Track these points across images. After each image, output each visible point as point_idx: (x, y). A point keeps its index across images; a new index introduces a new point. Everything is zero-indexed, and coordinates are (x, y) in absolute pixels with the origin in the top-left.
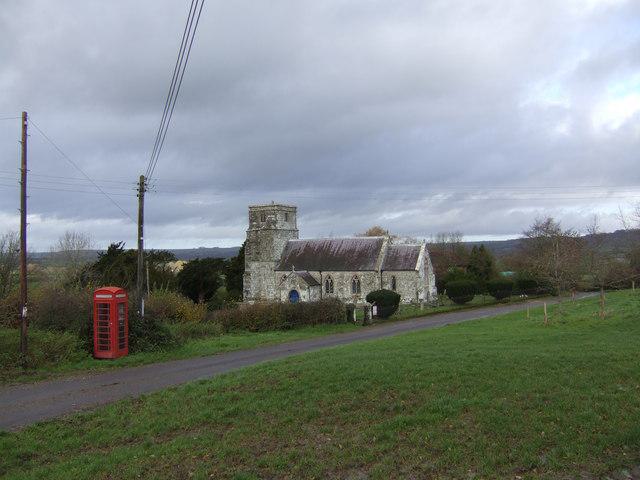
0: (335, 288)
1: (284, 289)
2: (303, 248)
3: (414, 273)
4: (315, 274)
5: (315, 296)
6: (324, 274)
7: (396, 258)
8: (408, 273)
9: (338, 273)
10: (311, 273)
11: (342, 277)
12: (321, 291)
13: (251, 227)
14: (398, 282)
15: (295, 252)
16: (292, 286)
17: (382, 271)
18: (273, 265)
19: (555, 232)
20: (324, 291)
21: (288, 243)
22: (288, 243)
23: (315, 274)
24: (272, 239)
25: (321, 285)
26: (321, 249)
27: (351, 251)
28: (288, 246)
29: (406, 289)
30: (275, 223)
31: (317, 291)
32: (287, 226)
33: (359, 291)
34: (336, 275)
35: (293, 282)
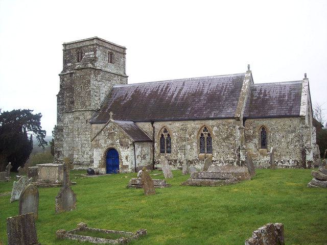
0: (174, 146)
1: (98, 146)
2: (130, 94)
3: (296, 121)
4: (146, 127)
5: (144, 158)
6: (158, 125)
7: (256, 89)
8: (287, 121)
9: (178, 124)
10: (140, 125)
11: (184, 130)
12: (153, 151)
13: (65, 69)
14: (270, 135)
15: (121, 99)
16: (110, 142)
17: (245, 119)
18: (88, 116)
19: (298, 163)
20: (157, 150)
21: (113, 90)
22: (113, 90)
23: (146, 127)
24: (89, 82)
25: (153, 142)
26: (154, 94)
27: (197, 94)
28: (112, 92)
29: (284, 145)
30: (94, 60)
31: (147, 149)
32: (111, 68)
33: (210, 150)
34: (174, 127)
35: (111, 135)
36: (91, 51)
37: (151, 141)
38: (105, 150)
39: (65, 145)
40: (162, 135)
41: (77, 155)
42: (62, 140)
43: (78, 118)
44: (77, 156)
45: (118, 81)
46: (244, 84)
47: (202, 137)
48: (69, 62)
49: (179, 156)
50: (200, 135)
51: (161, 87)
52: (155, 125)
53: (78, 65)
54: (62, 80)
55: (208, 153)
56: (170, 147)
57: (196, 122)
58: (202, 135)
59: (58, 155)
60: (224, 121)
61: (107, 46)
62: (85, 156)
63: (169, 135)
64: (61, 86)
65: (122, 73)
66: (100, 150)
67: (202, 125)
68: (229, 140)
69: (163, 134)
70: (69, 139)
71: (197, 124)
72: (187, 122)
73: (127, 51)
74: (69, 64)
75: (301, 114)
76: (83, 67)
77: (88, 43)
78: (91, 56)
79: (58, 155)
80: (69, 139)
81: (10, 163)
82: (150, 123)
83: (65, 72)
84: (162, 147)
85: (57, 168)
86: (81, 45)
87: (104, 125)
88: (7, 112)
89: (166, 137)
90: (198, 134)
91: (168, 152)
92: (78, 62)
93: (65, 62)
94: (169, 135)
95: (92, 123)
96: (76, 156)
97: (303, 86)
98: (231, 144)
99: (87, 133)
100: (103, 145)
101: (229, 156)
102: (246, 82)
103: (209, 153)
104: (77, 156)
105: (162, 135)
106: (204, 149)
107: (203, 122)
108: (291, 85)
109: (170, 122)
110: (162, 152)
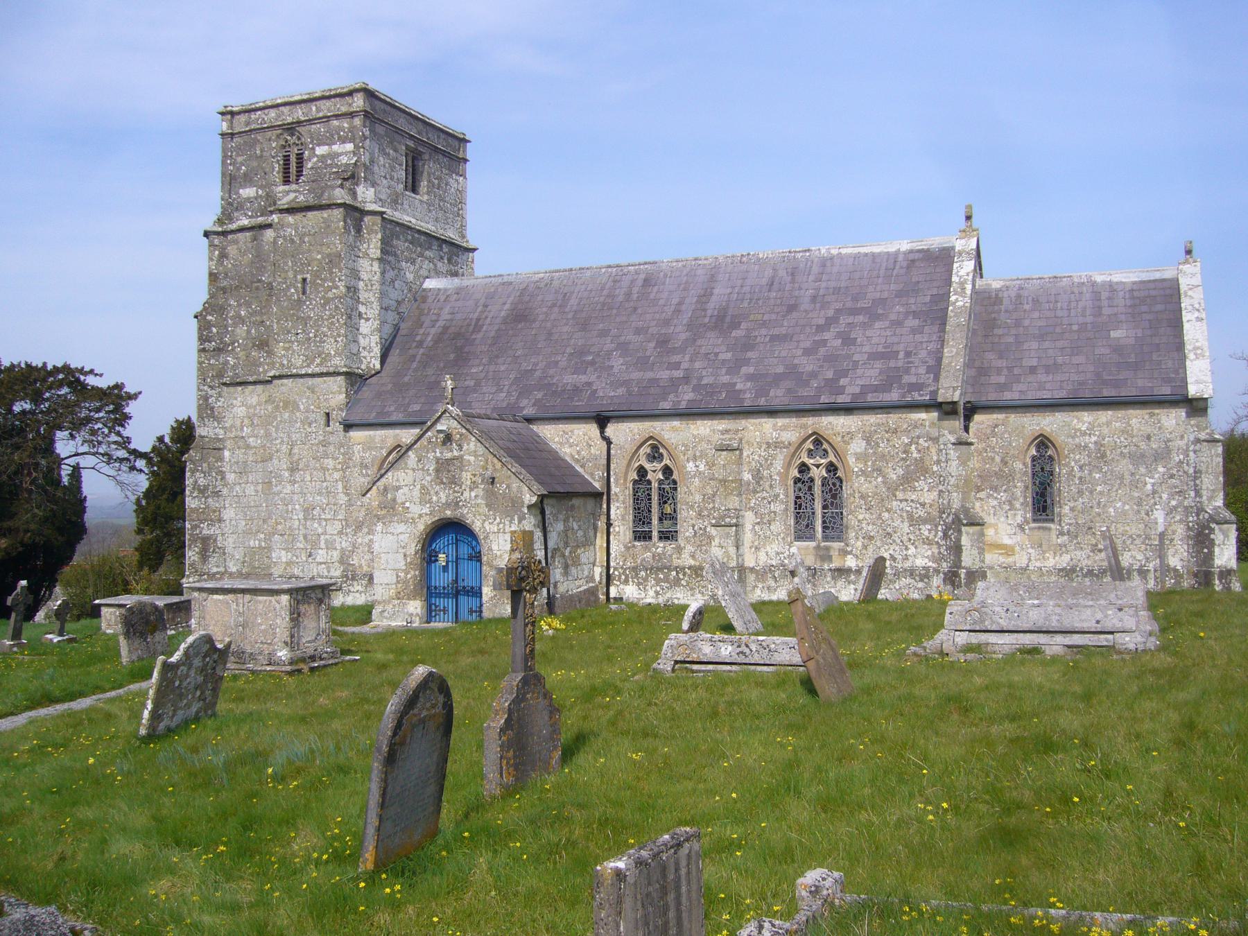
1: (390, 509)
3: (1172, 419)
6: (624, 433)
33: (834, 527)
36: (343, 140)
37: (597, 495)
38: (421, 527)
39: (228, 514)
40: (642, 472)
41: (287, 550)
42: (217, 494)
43: (289, 405)
44: (284, 556)
45: (439, 264)
46: (955, 279)
47: (803, 479)
48: (248, 180)
49: (716, 552)
50: (795, 473)
51: (625, 283)
52: (611, 430)
53: (287, 195)
54: (56, 370)
55: (826, 538)
56: (673, 517)
57: (780, 422)
58: (804, 468)
59: (204, 555)
60: (893, 419)
61: (402, 123)
62: (321, 555)
63: (667, 471)
64: (213, 277)
65: (451, 234)
66: (401, 528)
67: (803, 434)
68: (914, 489)
69: (648, 466)
70: (250, 490)
71: (784, 428)
72: (743, 423)
73: (471, 151)
74: (248, 192)
75: (1193, 391)
76: (312, 201)
77: (326, 108)
78: (344, 159)
79: (204, 555)
80: (250, 490)
81: (24, 583)
82: (592, 429)
83: (231, 220)
84: (641, 517)
85: (285, 598)
86: (299, 114)
87: (416, 431)
88: (13, 366)
89: (655, 476)
90: (788, 466)
91: (666, 536)
92: (286, 181)
93: (231, 181)
94: (667, 471)
95: (348, 426)
96: (281, 556)
97: (1183, 288)
98: (923, 505)
99: (330, 463)
100: (415, 509)
101: (912, 550)
102: (963, 269)
103: (832, 539)
104: (284, 556)
105: (642, 472)
106: (810, 526)
107: (811, 422)
108: (1134, 283)
109: (676, 423)
110: (642, 536)
